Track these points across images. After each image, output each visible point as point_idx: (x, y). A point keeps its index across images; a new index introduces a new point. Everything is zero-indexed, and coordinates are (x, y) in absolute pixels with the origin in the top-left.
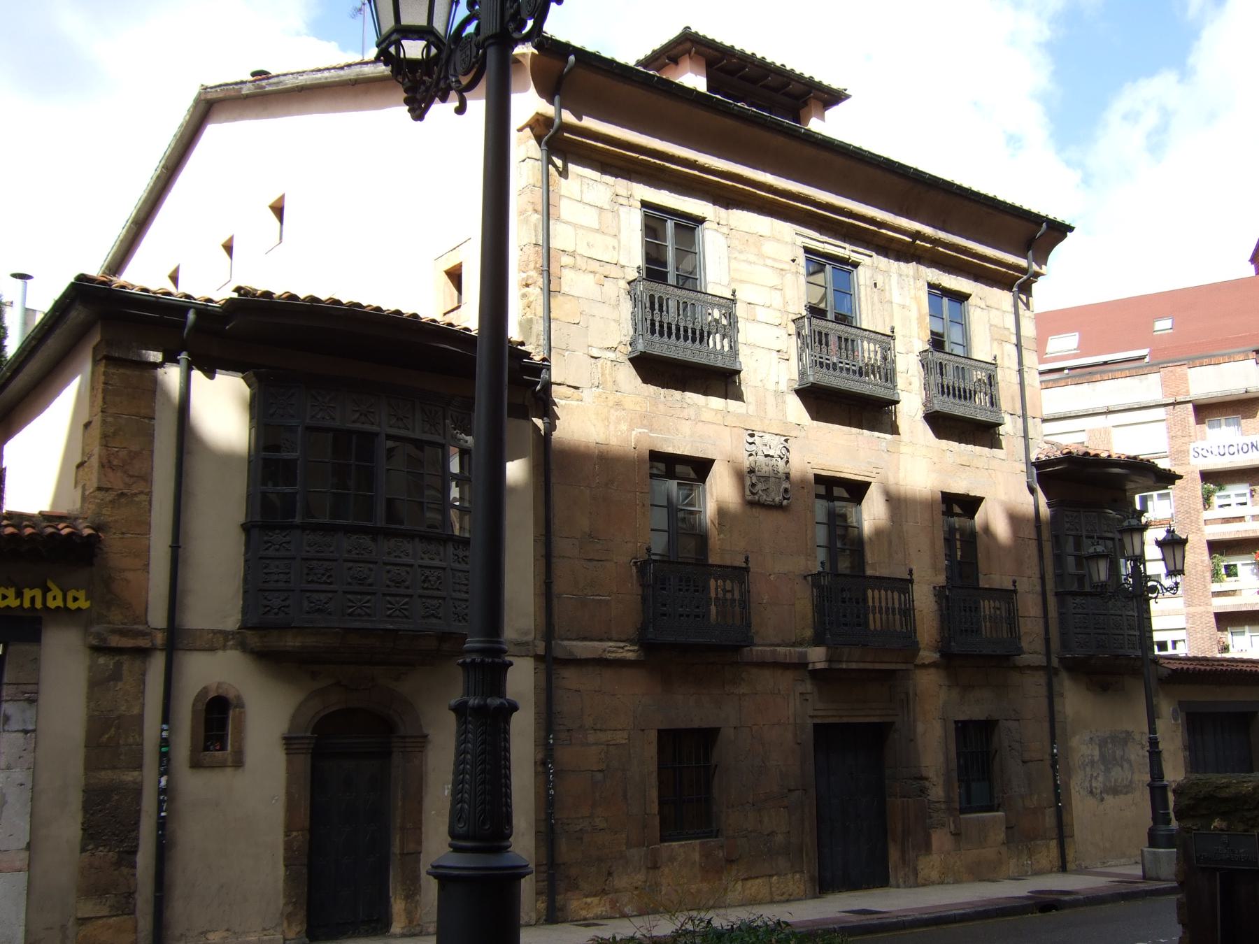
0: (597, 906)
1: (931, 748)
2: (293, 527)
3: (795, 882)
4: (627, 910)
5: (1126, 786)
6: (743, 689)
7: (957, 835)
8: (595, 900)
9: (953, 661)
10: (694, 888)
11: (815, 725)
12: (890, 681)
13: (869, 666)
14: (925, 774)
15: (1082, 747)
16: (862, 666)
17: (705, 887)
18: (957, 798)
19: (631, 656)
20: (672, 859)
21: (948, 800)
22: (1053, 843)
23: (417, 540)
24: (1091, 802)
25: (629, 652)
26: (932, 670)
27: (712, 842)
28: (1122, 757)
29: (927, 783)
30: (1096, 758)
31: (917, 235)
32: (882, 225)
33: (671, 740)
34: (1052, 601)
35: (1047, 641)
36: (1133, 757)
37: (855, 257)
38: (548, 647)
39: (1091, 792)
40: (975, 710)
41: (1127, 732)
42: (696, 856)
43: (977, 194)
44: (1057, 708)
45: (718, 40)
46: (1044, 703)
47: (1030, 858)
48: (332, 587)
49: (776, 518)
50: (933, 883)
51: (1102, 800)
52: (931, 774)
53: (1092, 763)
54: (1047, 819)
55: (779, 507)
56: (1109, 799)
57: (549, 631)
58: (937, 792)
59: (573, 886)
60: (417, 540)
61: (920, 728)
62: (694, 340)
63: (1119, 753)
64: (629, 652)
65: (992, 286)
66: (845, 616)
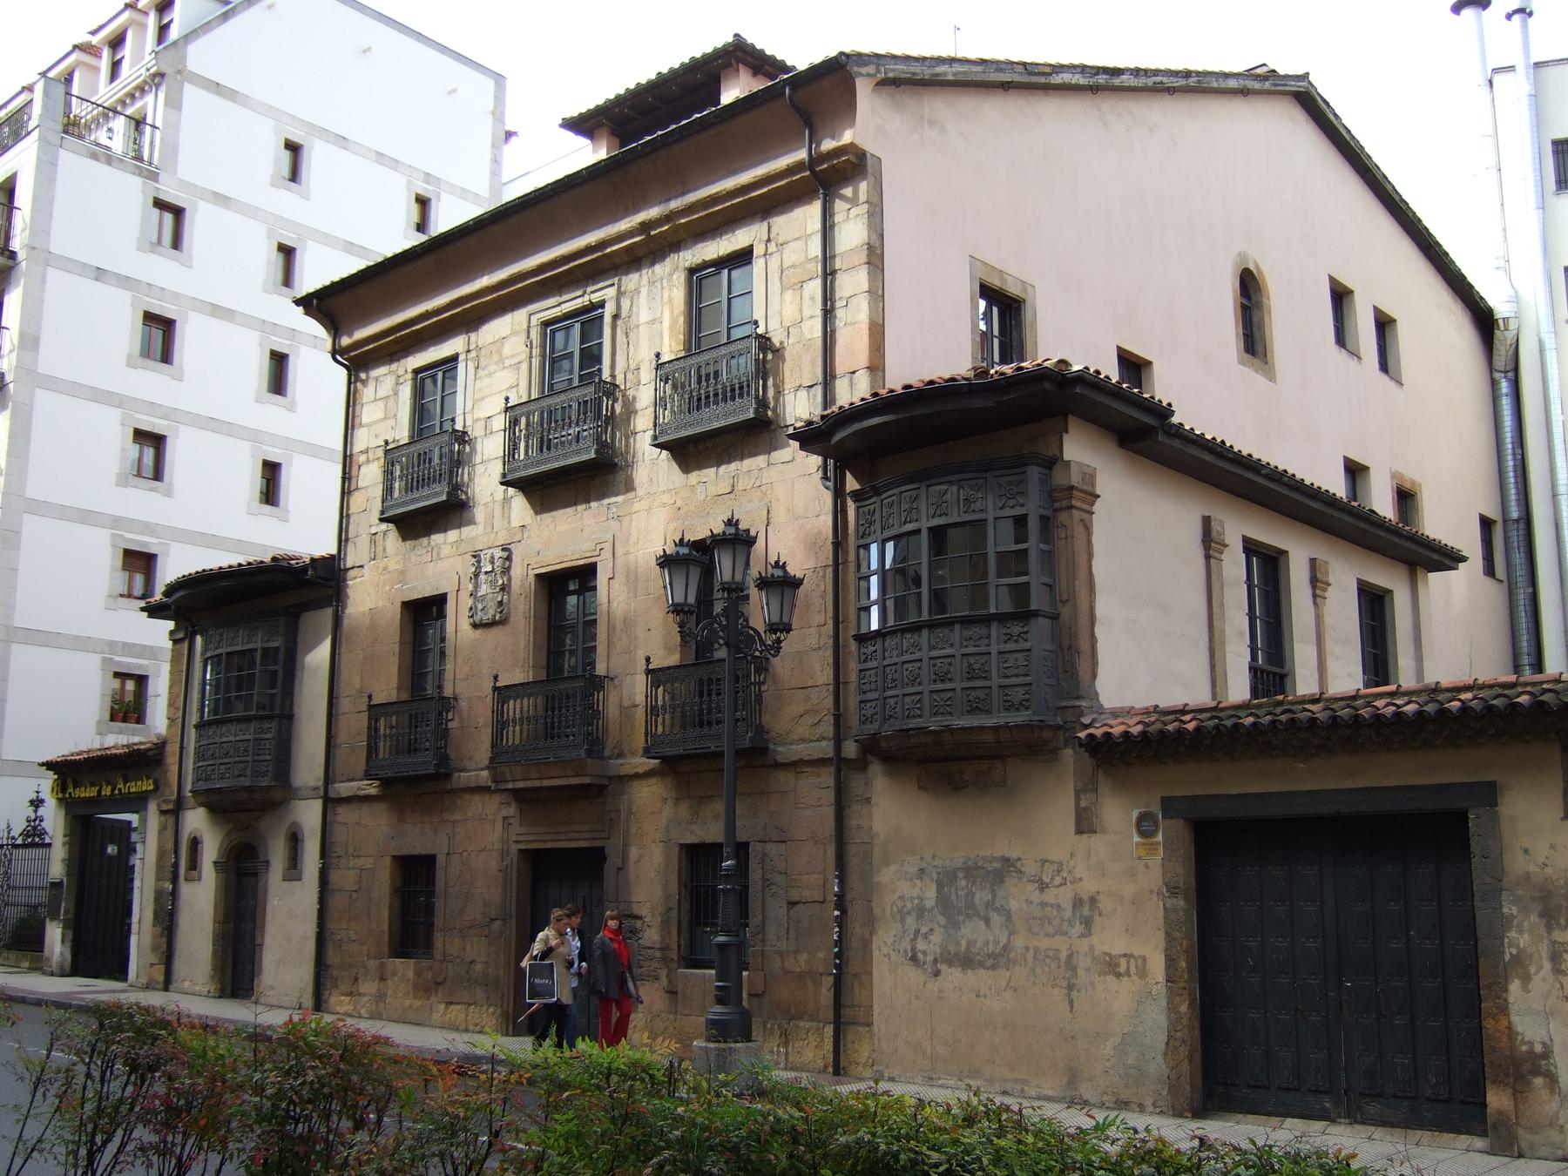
1: (648, 878)
3: (488, 1016)
4: (363, 1012)
5: (991, 955)
6: (457, 816)
7: (672, 993)
8: (347, 999)
9: (682, 768)
11: (520, 851)
12: (599, 793)
13: (537, 784)
14: (636, 910)
15: (900, 885)
16: (529, 784)
17: (417, 1003)
18: (675, 946)
19: (373, 791)
20: (394, 974)
21: (664, 949)
22: (829, 1030)
23: (957, 627)
24: (912, 974)
25: (370, 788)
26: (653, 781)
27: (425, 963)
28: (989, 905)
30: (929, 903)
31: (645, 227)
32: (602, 245)
34: (192, 734)
36: (1014, 905)
37: (596, 298)
39: (914, 959)
40: (710, 830)
41: (1006, 860)
42: (411, 974)
43: (343, 281)
44: (855, 819)
45: (584, 110)
46: (829, 812)
47: (786, 1044)
48: (948, 686)
51: (937, 974)
52: (644, 910)
53: (921, 911)
54: (824, 990)
56: (953, 976)
57: (328, 778)
58: (651, 935)
60: (957, 627)
61: (634, 852)
62: (733, 399)
63: (981, 896)
65: (791, 209)
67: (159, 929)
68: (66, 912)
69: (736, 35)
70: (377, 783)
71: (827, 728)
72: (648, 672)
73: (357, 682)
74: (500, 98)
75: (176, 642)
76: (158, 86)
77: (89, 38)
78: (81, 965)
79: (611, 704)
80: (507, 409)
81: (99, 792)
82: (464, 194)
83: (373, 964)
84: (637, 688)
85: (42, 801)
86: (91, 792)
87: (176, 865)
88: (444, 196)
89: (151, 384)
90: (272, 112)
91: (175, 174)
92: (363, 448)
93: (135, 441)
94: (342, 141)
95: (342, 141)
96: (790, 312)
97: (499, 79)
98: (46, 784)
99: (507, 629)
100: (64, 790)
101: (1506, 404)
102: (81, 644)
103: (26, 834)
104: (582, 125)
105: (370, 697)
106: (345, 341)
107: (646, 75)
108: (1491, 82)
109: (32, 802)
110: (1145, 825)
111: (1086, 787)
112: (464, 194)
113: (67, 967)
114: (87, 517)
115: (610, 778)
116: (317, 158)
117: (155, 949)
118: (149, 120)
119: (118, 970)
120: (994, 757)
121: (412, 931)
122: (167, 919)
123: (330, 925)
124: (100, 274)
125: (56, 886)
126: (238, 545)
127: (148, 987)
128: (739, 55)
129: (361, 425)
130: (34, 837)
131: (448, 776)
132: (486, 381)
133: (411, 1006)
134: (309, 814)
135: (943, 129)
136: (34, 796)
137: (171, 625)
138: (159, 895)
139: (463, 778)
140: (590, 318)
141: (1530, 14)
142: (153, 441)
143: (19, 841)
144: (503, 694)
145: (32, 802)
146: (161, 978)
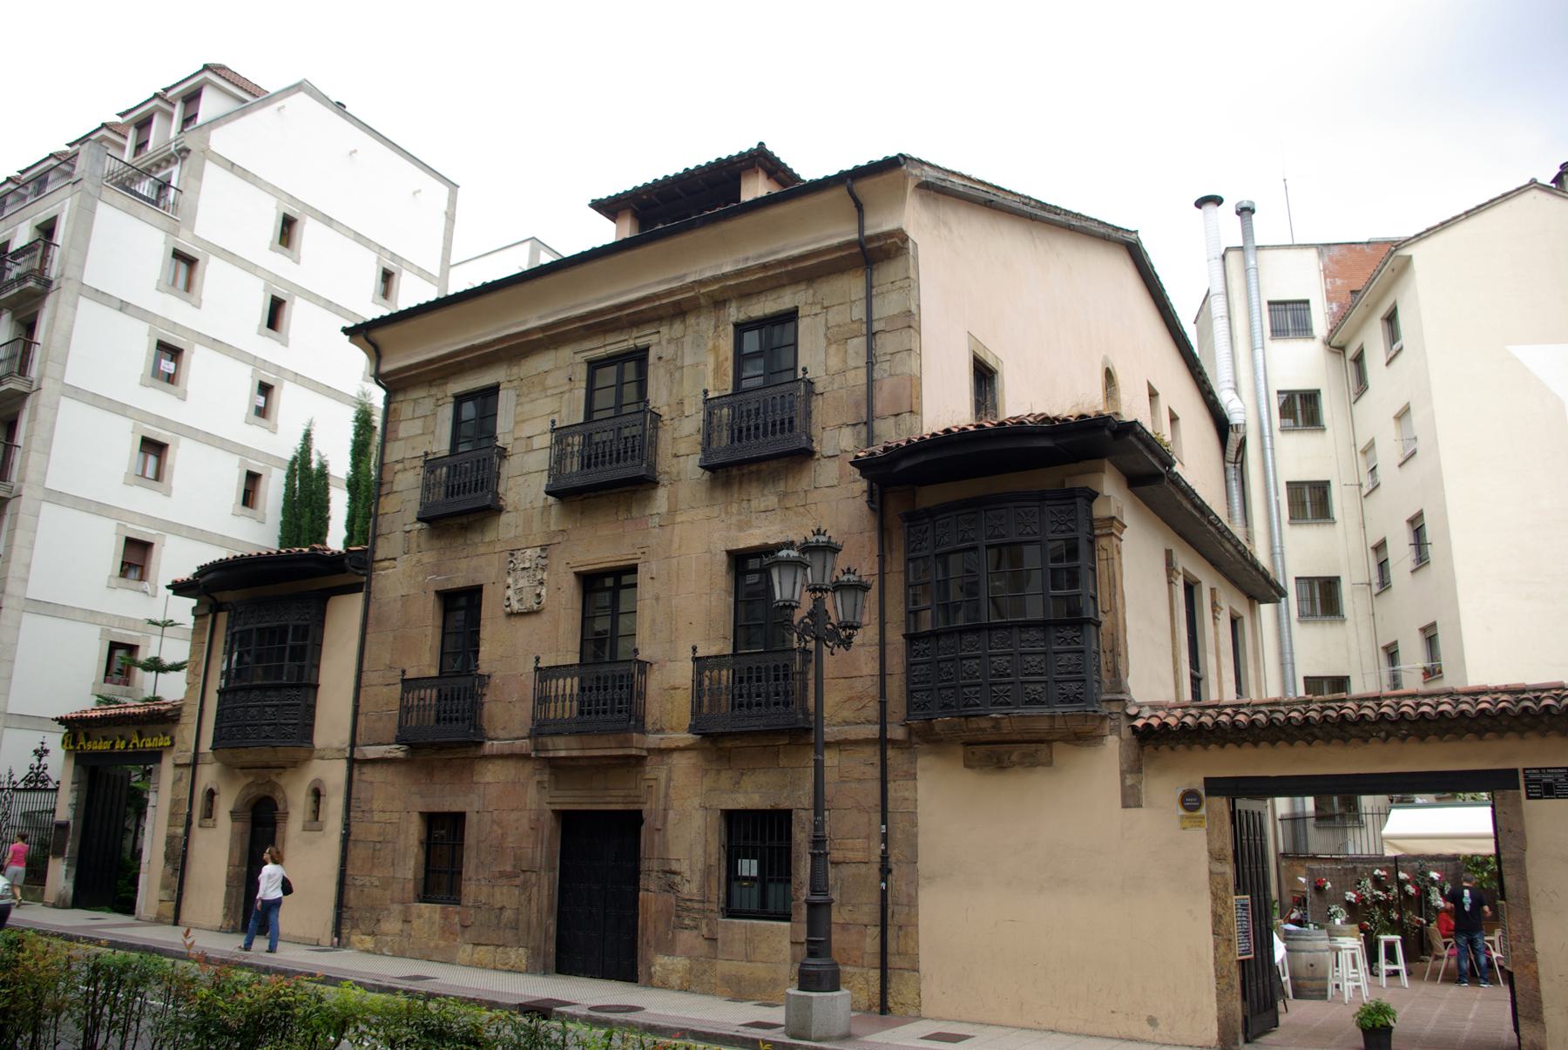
0: (369, 942)
2: (251, 689)
8: (368, 938)
9: (719, 740)
10: (432, 944)
14: (675, 866)
17: (442, 943)
19: (400, 754)
25: (397, 751)
26: (692, 754)
27: (451, 908)
29: (678, 879)
33: (432, 820)
35: (883, 704)
37: (641, 342)
38: (352, 752)
40: (752, 794)
42: (437, 917)
49: (533, 621)
50: (672, 988)
52: (683, 867)
55: (537, 612)
59: (355, 926)
64: (397, 751)
66: (777, 694)
67: (170, 869)
68: (71, 851)
69: (761, 144)
70: (405, 747)
71: (872, 711)
72: (696, 660)
73: (386, 658)
74: (452, 202)
75: (197, 617)
76: (184, 159)
77: (120, 120)
78: (85, 895)
79: (654, 684)
80: (553, 430)
81: (113, 745)
82: (422, 273)
83: (396, 908)
84: (683, 672)
85: (46, 751)
86: (104, 746)
87: (190, 816)
88: (404, 272)
89: (158, 402)
90: (273, 190)
91: (192, 229)
92: (399, 457)
93: (142, 450)
94: (328, 221)
95: (328, 221)
96: (834, 362)
97: (453, 187)
98: (55, 740)
99: (545, 617)
100: (75, 743)
101: (1234, 486)
102: (90, 616)
103: (27, 780)
104: (608, 207)
105: (404, 672)
106: (385, 368)
107: (674, 167)
108: (1224, 257)
109: (36, 752)
110: (1190, 801)
111: (1134, 767)
112: (422, 273)
113: (69, 901)
114: (100, 509)
115: (649, 750)
116: (308, 231)
117: (164, 887)
118: (173, 183)
119: (126, 906)
120: (1041, 741)
121: (441, 874)
122: (179, 858)
123: (349, 871)
124: (123, 306)
125: (62, 827)
126: (221, 541)
127: (159, 920)
128: (760, 160)
129: (397, 439)
130: (37, 781)
131: (481, 744)
132: (527, 407)
133: (437, 947)
134: (333, 774)
135: (950, 230)
136: (39, 746)
137: (193, 602)
138: (170, 839)
139: (490, 747)
140: (639, 357)
141: (1253, 211)
142: (153, 448)
143: (21, 786)
144: (545, 674)
145: (36, 752)
146: (171, 913)
